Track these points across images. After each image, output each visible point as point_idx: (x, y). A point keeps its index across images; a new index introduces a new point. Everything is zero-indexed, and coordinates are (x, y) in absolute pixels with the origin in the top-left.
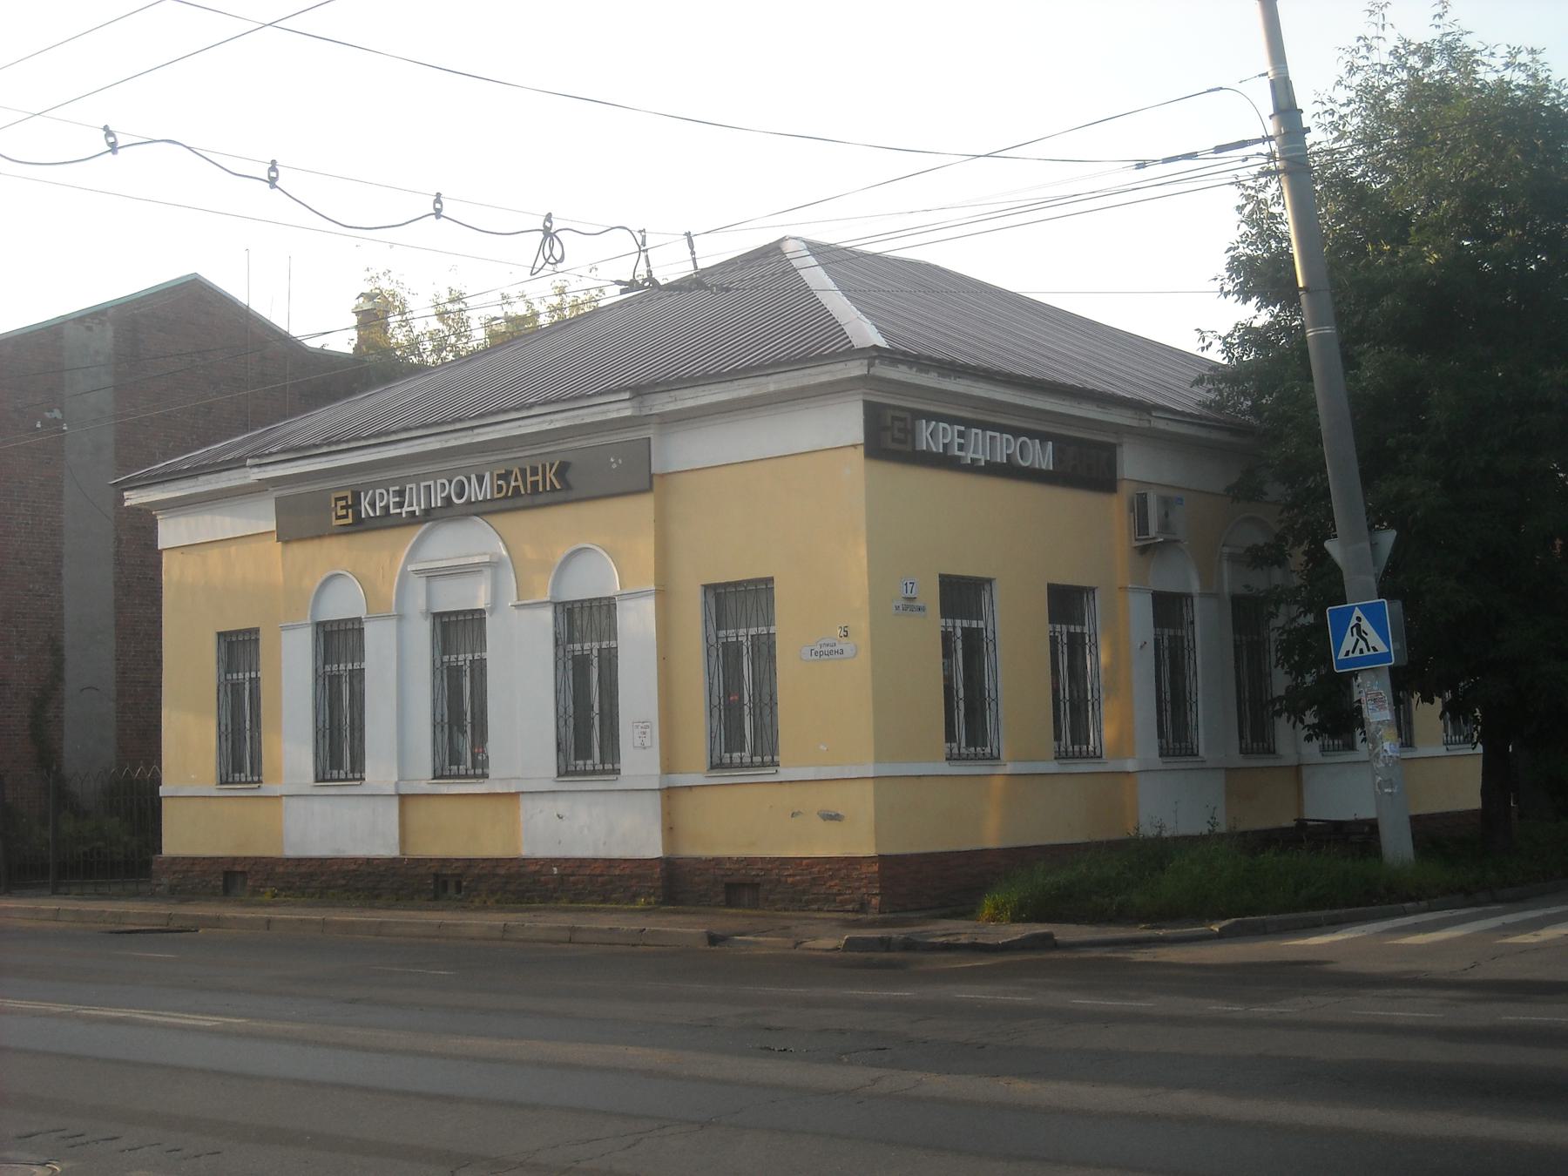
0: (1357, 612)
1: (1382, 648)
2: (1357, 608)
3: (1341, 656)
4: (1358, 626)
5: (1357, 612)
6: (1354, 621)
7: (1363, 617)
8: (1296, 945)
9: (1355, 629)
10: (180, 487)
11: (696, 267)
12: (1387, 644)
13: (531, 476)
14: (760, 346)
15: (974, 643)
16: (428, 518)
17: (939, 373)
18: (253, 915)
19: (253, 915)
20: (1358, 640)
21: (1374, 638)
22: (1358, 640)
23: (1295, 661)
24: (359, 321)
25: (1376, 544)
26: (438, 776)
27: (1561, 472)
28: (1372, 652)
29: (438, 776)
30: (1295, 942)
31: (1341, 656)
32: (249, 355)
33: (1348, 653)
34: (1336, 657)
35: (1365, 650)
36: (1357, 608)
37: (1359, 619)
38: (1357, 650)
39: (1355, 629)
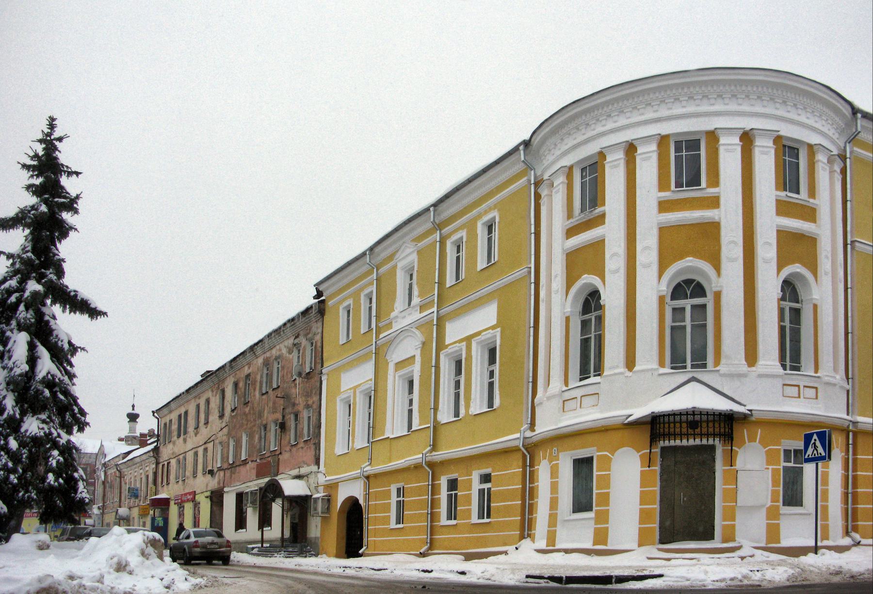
0: (815, 437)
1: (823, 454)
3: (806, 457)
4: (814, 443)
5: (815, 437)
6: (813, 441)
12: (825, 452)
13: (597, 471)
15: (796, 313)
16: (347, 400)
17: (774, 582)
18: (766, 370)
19: (766, 370)
24: (61, 303)
25: (687, 412)
27: (62, 479)
28: (819, 455)
33: (809, 455)
37: (815, 440)
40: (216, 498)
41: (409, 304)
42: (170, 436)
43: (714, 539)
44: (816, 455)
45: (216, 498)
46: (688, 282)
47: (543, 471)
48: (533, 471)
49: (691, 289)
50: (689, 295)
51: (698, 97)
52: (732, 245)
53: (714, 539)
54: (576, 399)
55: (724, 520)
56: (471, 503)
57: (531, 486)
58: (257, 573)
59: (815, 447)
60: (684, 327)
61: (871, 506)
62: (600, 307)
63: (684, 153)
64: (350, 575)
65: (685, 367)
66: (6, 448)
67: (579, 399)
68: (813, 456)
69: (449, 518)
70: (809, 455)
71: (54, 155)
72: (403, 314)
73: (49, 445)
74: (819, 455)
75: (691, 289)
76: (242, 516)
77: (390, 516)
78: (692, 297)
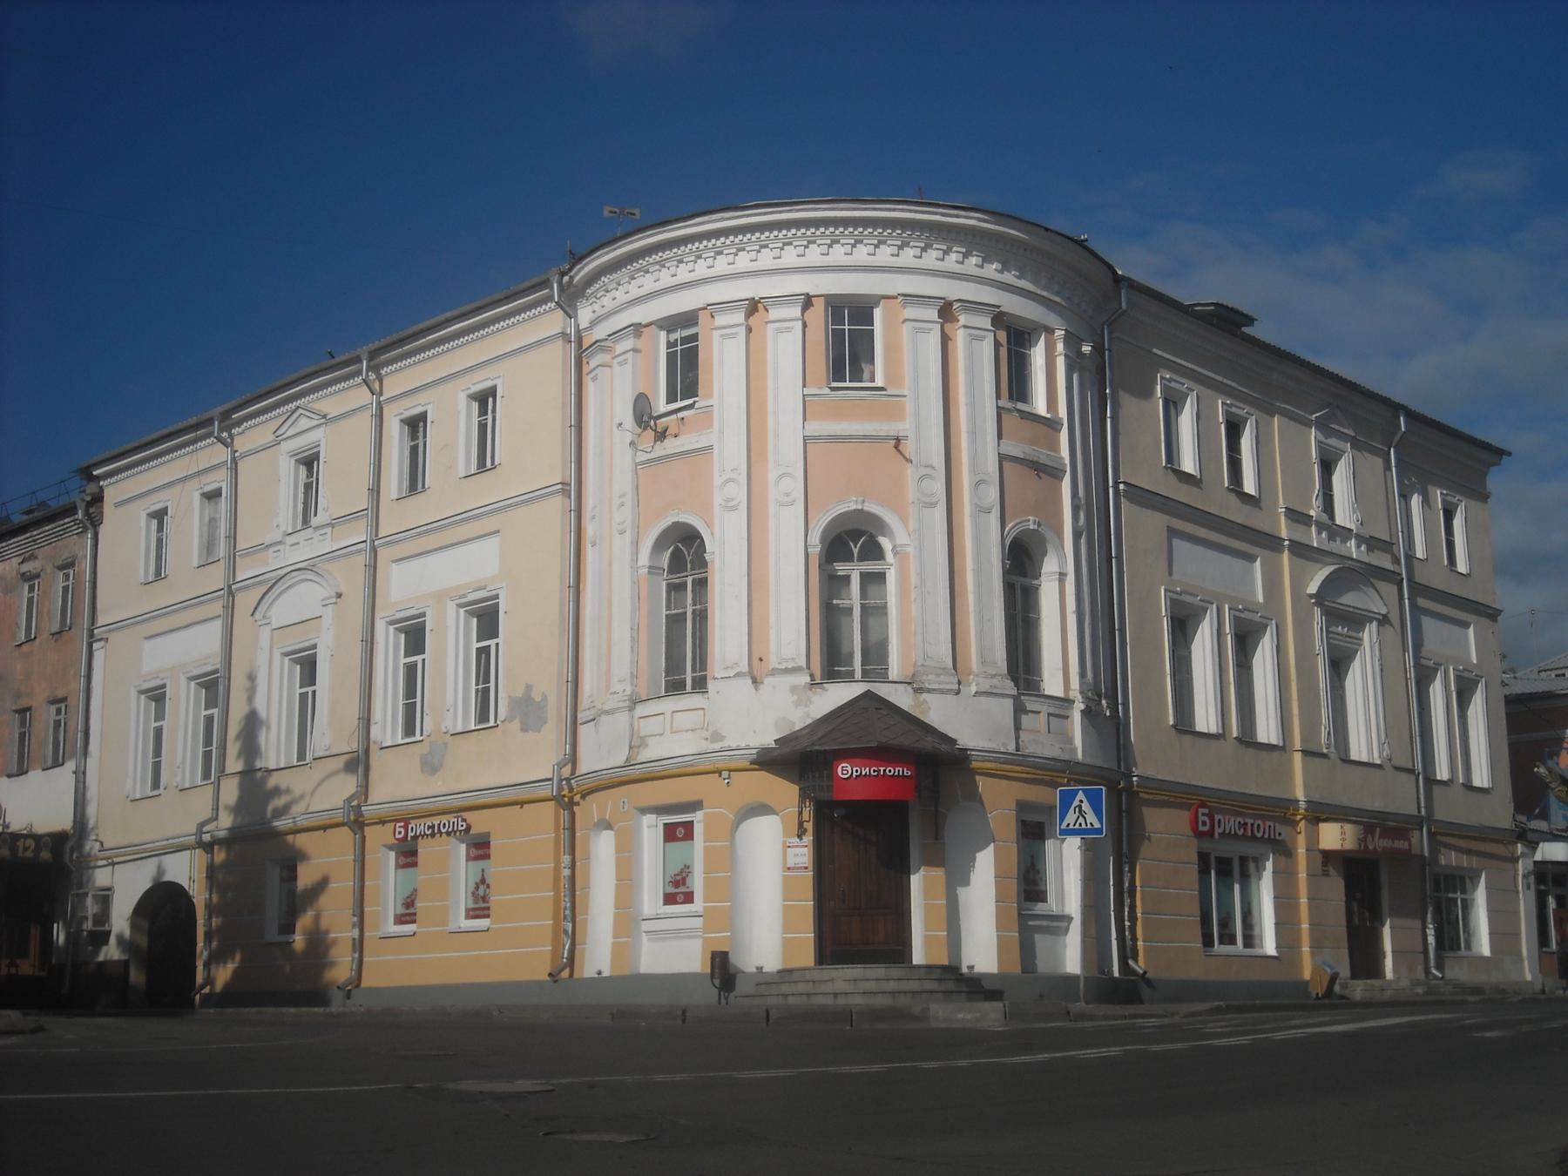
0: (1080, 796)
1: (1097, 825)
2: (1080, 792)
3: (1063, 826)
4: (1080, 807)
5: (1080, 796)
6: (1076, 803)
7: (1084, 800)
8: (1022, 233)
9: (1077, 809)
11: (1420, 953)
12: (1101, 822)
14: (22, 547)
20: (1078, 817)
21: (1091, 818)
22: (1078, 817)
23: (1343, 628)
26: (1216, 858)
29: (1216, 858)
30: (1017, 233)
31: (1063, 826)
32: (23, 639)
33: (1069, 824)
34: (1060, 825)
36: (1080, 792)
38: (1077, 826)
39: (1077, 809)
40: (1252, 825)
41: (306, 521)
44: (1084, 826)
45: (1252, 825)
46: (856, 534)
47: (602, 849)
49: (859, 545)
50: (856, 555)
51: (872, 242)
52: (982, 486)
54: (662, 717)
55: (489, 687)
56: (1227, 859)
59: (1082, 813)
60: (850, 610)
61: (945, 933)
62: (702, 563)
63: (847, 327)
64: (1256, 932)
67: (668, 716)
68: (1077, 826)
69: (474, 913)
70: (1069, 824)
71: (864, 366)
72: (293, 539)
74: (1089, 826)
75: (859, 545)
76: (555, 893)
78: (862, 558)
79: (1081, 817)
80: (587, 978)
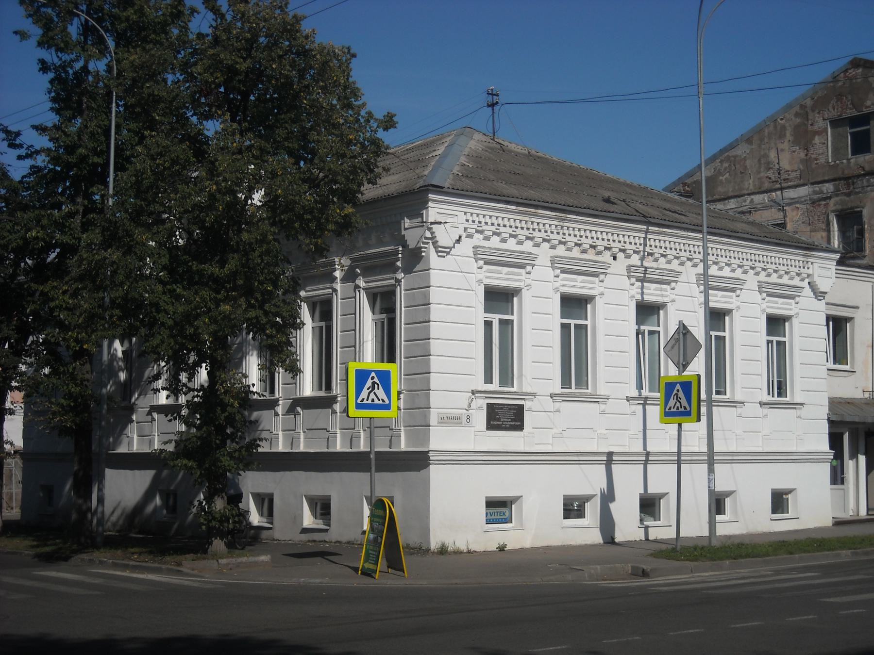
0: (678, 387)
4: (677, 394)
5: (678, 387)
6: (675, 392)
10: (315, 345)
33: (670, 408)
35: (376, 399)
37: (678, 391)
38: (676, 407)
42: (368, 271)
43: (485, 383)
48: (843, 477)
53: (485, 383)
57: (587, 579)
58: (767, 250)
59: (678, 399)
65: (461, 423)
66: (1, 276)
73: (245, 325)
77: (868, 131)
79: (678, 403)
80: (3, 420)
